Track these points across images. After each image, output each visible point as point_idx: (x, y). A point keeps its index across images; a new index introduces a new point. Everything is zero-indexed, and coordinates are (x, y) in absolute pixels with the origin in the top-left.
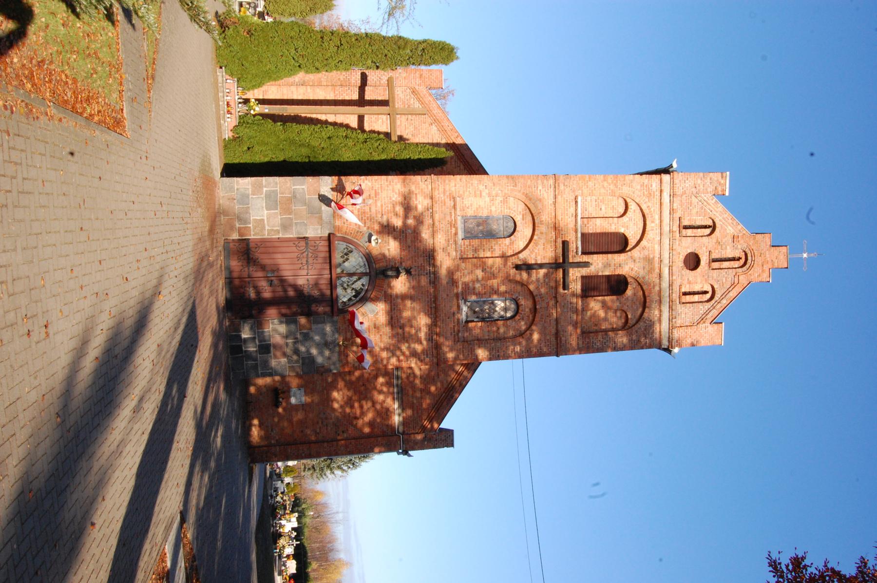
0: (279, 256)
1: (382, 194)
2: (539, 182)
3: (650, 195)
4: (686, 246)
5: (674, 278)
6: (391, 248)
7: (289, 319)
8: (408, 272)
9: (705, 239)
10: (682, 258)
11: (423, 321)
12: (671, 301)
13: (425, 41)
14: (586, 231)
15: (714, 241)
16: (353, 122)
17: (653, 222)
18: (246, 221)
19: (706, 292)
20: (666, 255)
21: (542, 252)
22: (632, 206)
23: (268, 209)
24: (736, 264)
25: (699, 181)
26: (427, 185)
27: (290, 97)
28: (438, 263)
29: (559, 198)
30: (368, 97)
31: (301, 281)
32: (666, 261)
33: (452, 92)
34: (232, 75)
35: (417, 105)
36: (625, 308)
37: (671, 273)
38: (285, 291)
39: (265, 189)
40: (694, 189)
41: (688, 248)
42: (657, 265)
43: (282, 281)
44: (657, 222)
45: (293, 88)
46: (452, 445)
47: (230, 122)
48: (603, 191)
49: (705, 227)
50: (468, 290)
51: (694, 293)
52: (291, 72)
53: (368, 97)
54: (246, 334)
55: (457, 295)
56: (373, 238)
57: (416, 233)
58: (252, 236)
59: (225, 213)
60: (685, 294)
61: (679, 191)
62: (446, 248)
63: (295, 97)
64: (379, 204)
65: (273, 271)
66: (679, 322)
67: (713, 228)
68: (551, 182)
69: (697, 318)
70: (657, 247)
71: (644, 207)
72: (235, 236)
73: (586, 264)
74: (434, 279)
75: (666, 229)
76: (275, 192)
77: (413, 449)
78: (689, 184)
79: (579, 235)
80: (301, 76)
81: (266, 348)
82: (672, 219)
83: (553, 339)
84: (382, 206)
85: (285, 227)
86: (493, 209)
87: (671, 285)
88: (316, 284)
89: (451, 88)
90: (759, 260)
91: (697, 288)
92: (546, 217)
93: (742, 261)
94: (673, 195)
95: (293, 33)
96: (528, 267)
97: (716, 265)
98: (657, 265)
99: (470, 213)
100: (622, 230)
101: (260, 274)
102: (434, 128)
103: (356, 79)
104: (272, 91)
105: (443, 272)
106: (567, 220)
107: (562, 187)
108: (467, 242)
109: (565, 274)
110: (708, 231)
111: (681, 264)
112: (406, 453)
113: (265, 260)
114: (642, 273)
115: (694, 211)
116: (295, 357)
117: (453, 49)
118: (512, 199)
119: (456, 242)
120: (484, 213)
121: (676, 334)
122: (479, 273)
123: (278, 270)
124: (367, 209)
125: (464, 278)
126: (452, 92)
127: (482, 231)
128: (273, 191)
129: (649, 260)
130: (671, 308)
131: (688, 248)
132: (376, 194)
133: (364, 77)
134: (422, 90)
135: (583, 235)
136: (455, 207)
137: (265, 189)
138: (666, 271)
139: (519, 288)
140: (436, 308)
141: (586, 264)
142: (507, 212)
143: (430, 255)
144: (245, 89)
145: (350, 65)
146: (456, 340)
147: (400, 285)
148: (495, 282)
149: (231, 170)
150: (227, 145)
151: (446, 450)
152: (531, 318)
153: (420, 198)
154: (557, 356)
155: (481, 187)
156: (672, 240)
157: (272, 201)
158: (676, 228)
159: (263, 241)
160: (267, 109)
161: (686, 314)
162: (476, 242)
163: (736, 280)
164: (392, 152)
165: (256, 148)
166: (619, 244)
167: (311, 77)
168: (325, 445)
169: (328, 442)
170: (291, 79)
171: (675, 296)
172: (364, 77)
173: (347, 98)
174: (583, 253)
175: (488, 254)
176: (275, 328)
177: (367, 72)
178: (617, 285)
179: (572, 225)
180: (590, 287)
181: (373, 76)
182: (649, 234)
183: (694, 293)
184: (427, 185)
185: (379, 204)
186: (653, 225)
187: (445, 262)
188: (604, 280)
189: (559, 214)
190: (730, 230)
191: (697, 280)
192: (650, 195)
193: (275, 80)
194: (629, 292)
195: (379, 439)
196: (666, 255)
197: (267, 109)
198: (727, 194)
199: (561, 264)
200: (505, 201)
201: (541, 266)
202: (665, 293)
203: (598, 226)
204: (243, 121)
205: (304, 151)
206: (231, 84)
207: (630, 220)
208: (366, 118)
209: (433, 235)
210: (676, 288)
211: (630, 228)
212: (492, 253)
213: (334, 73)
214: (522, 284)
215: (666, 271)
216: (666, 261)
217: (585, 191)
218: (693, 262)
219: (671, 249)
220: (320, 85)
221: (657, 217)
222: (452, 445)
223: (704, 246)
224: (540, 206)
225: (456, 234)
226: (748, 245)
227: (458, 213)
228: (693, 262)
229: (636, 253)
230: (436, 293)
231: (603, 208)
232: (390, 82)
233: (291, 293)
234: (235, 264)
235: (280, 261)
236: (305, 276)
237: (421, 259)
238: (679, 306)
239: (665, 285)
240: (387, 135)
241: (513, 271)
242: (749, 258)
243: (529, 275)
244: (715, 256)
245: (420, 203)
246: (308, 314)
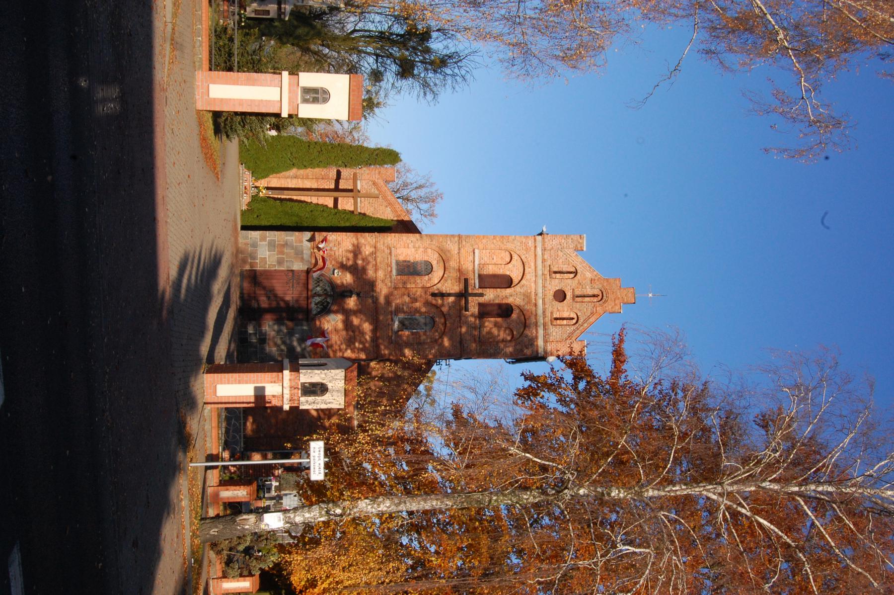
0: (274, 281)
1: (340, 244)
3: (527, 250)
4: (555, 284)
6: (348, 278)
7: (279, 321)
8: (358, 295)
9: (569, 281)
10: (552, 293)
11: (367, 327)
12: (545, 325)
13: (378, 149)
14: (485, 272)
16: (330, 202)
18: (254, 258)
20: (540, 291)
21: (452, 286)
22: (515, 257)
23: (269, 251)
24: (595, 299)
27: (286, 186)
28: (378, 290)
29: (462, 250)
30: (341, 187)
31: (288, 298)
32: (540, 295)
33: (441, 196)
34: (249, 169)
35: (377, 192)
36: (511, 327)
37: (544, 303)
38: (278, 304)
42: (533, 297)
43: (276, 296)
44: (533, 267)
45: (289, 180)
47: (246, 199)
48: (493, 246)
49: (571, 273)
50: (398, 310)
51: (563, 319)
52: (288, 168)
53: (341, 187)
54: (251, 330)
55: (391, 312)
56: (336, 271)
57: (364, 270)
58: (258, 268)
59: (242, 252)
60: (556, 319)
61: (548, 245)
62: (384, 282)
63: (290, 186)
65: (270, 291)
66: (551, 338)
67: (576, 273)
68: (456, 239)
69: (565, 336)
70: (533, 285)
71: (523, 257)
72: (247, 267)
73: (481, 295)
74: (375, 301)
75: (540, 273)
76: (274, 241)
78: (555, 242)
79: (477, 275)
80: (294, 171)
81: (263, 340)
82: (544, 266)
83: (458, 345)
85: (280, 262)
86: (417, 256)
87: (544, 312)
88: (297, 301)
89: (439, 192)
90: (611, 296)
91: (566, 315)
92: (453, 264)
93: (600, 298)
94: (544, 250)
95: (290, 143)
96: (442, 295)
98: (533, 297)
99: (401, 258)
100: (508, 273)
101: (263, 292)
102: (389, 209)
103: (333, 173)
104: (274, 181)
105: (382, 300)
106: (467, 266)
107: (464, 243)
108: (399, 277)
109: (467, 302)
110: (572, 275)
111: (552, 297)
113: (266, 283)
114: (522, 303)
115: (561, 261)
116: (283, 347)
117: (398, 154)
118: (429, 250)
119: (391, 277)
120: (412, 259)
121: (549, 348)
122: (407, 299)
123: (273, 290)
124: (332, 253)
125: (397, 301)
126: (441, 196)
127: (409, 270)
129: (527, 296)
130: (545, 329)
132: (339, 244)
133: (339, 173)
134: (381, 182)
135: (480, 276)
136: (390, 253)
138: (540, 302)
139: (433, 310)
142: (426, 258)
143: (372, 284)
144: (257, 179)
145: (327, 164)
146: (391, 342)
147: (351, 302)
148: (418, 305)
149: (244, 228)
150: (243, 213)
153: (368, 248)
155: (408, 241)
157: (272, 245)
158: (547, 272)
159: (265, 271)
160: (270, 193)
161: (555, 332)
162: (405, 278)
164: (354, 222)
165: (262, 217)
166: (507, 282)
167: (302, 172)
170: (287, 173)
171: (548, 319)
172: (339, 173)
173: (326, 187)
174: (480, 287)
175: (413, 286)
176: (269, 327)
177: (340, 169)
178: (505, 311)
179: (471, 268)
180: (485, 311)
181: (346, 173)
182: (527, 276)
183: (563, 319)
187: (382, 290)
188: (495, 308)
189: (462, 260)
190: (589, 275)
191: (564, 310)
192: (527, 250)
193: (277, 173)
194: (514, 316)
196: (540, 291)
197: (270, 193)
198: (585, 249)
199: (464, 295)
200: (425, 251)
201: (449, 295)
202: (541, 321)
203: (491, 270)
204: (255, 198)
205: (295, 219)
206: (248, 175)
207: (514, 266)
208: (340, 200)
209: (376, 270)
210: (548, 314)
211: (514, 272)
212: (417, 285)
213: (317, 170)
214: (436, 307)
215: (540, 302)
216: (540, 295)
217: (481, 246)
218: (560, 296)
219: (544, 287)
220: (307, 178)
221: (533, 264)
223: (568, 285)
224: (448, 255)
225: (391, 271)
227: (393, 258)
228: (560, 296)
229: (518, 288)
230: (374, 310)
232: (355, 175)
233: (282, 304)
234: (246, 285)
235: (275, 285)
236: (290, 294)
238: (551, 327)
239: (540, 312)
240: (352, 212)
241: (430, 298)
243: (443, 300)
244: (577, 293)
245: (367, 250)
246: (291, 319)
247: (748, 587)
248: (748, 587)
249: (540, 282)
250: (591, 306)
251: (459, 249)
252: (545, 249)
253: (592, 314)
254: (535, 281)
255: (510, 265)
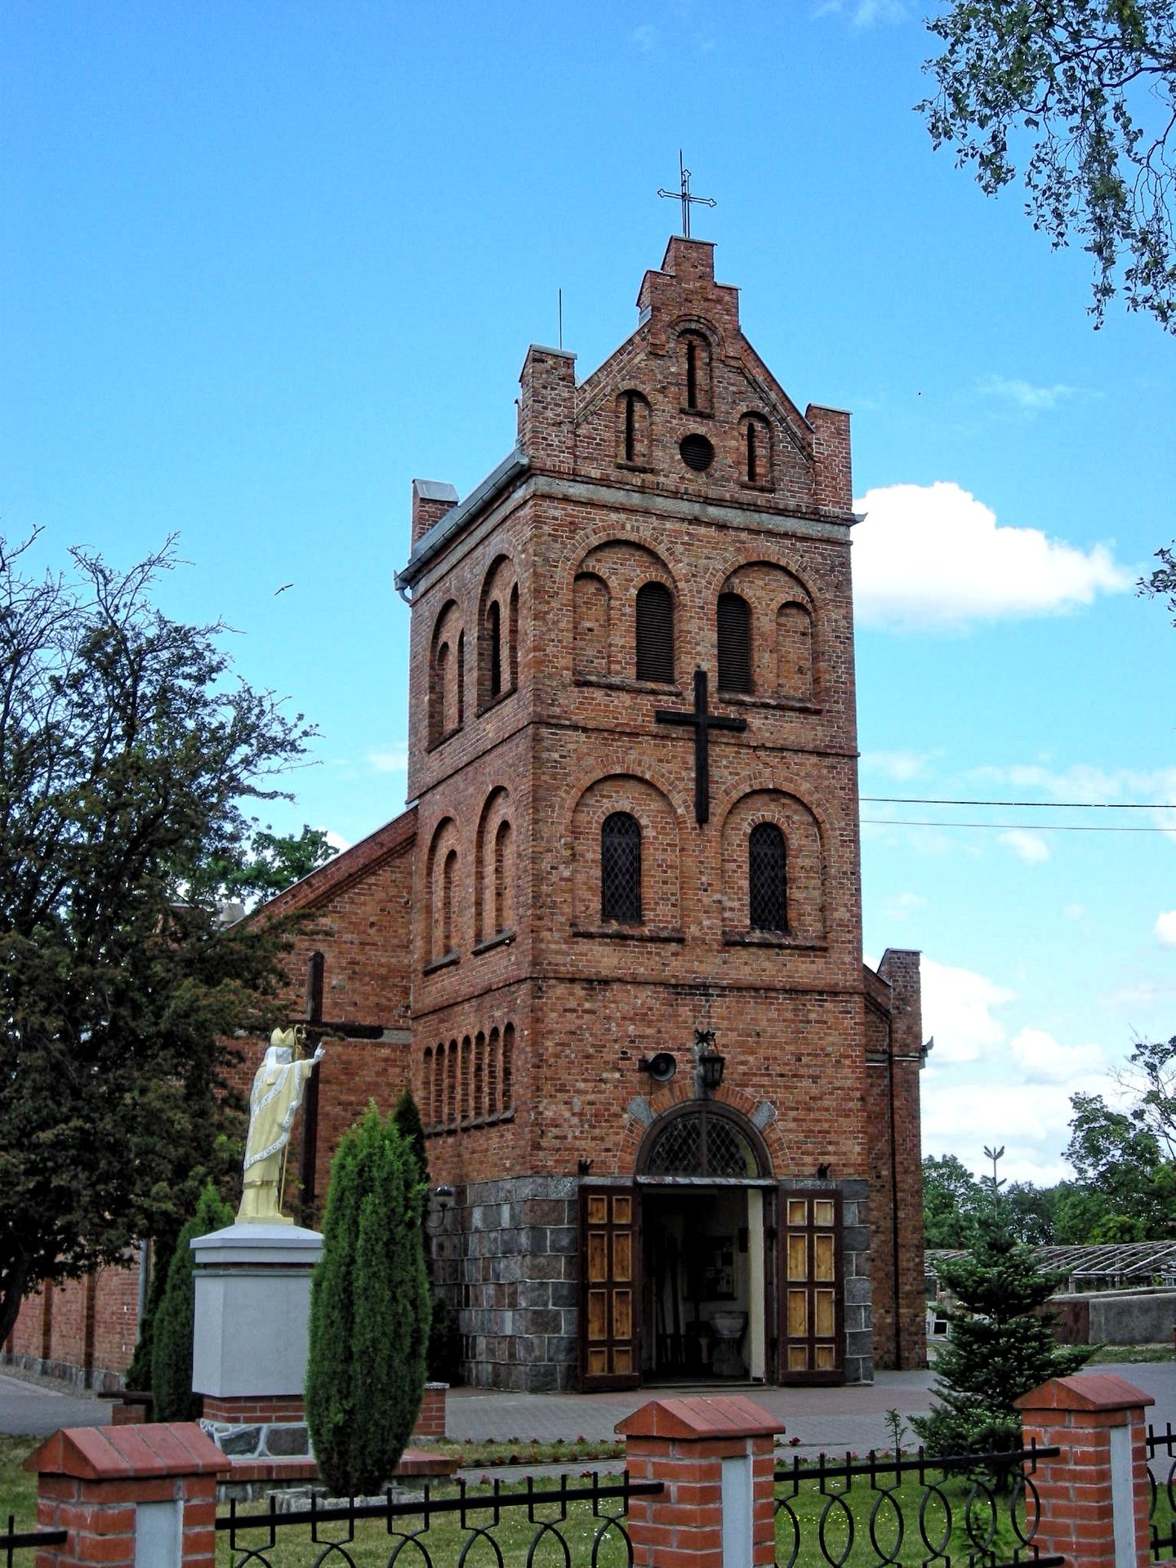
2: (545, 755)
5: (727, 496)
15: (660, 397)
17: (623, 527)
19: (751, 428)
25: (549, 414)
26: (549, 987)
29: (578, 718)
39: (550, 1307)
40: (565, 428)
41: (672, 458)
44: (623, 516)
46: (916, 954)
64: (581, 1085)
67: (633, 396)
68: (544, 731)
69: (800, 459)
71: (595, 541)
73: (700, 677)
77: (918, 1036)
82: (620, 485)
84: (585, 1081)
90: (697, 308)
93: (697, 342)
94: (575, 476)
97: (701, 402)
100: (634, 592)
110: (638, 407)
111: (702, 478)
112: (923, 1050)
128: (555, 1290)
131: (672, 458)
137: (550, 1307)
140: (767, 989)
141: (700, 677)
151: (925, 968)
152: (787, 801)
154: (854, 757)
156: (658, 490)
163: (733, 363)
168: (901, 1214)
169: (896, 1209)
184: (549, 987)
185: (581, 1085)
186: (628, 527)
195: (897, 1103)
207: (615, 572)
211: (626, 577)
218: (697, 452)
219: (675, 495)
221: (614, 516)
222: (916, 954)
226: (671, 325)
228: (697, 452)
231: (588, 625)
237: (681, 1010)
242: (693, 326)
247: (1072, 1199)
248: (1072, 1199)
249: (662, 504)
250: (719, 370)
251: (575, 728)
252: (816, 512)
253: (741, 371)
254: (662, 517)
255: (613, 583)
